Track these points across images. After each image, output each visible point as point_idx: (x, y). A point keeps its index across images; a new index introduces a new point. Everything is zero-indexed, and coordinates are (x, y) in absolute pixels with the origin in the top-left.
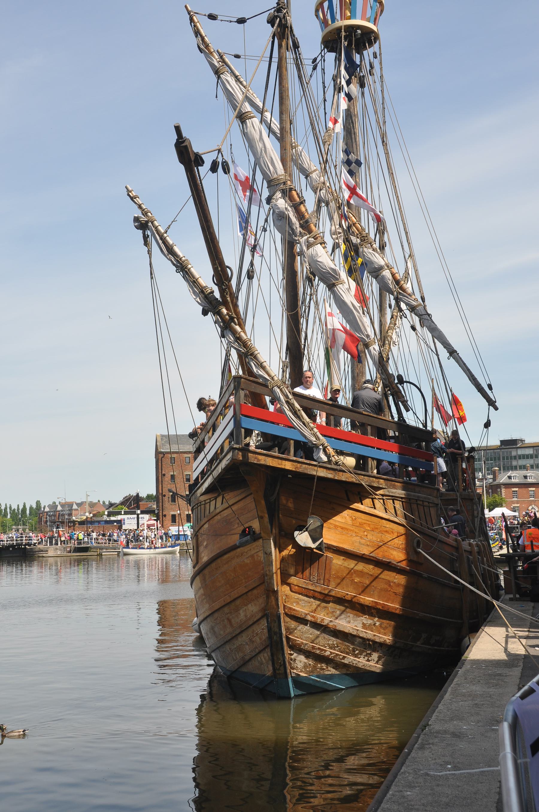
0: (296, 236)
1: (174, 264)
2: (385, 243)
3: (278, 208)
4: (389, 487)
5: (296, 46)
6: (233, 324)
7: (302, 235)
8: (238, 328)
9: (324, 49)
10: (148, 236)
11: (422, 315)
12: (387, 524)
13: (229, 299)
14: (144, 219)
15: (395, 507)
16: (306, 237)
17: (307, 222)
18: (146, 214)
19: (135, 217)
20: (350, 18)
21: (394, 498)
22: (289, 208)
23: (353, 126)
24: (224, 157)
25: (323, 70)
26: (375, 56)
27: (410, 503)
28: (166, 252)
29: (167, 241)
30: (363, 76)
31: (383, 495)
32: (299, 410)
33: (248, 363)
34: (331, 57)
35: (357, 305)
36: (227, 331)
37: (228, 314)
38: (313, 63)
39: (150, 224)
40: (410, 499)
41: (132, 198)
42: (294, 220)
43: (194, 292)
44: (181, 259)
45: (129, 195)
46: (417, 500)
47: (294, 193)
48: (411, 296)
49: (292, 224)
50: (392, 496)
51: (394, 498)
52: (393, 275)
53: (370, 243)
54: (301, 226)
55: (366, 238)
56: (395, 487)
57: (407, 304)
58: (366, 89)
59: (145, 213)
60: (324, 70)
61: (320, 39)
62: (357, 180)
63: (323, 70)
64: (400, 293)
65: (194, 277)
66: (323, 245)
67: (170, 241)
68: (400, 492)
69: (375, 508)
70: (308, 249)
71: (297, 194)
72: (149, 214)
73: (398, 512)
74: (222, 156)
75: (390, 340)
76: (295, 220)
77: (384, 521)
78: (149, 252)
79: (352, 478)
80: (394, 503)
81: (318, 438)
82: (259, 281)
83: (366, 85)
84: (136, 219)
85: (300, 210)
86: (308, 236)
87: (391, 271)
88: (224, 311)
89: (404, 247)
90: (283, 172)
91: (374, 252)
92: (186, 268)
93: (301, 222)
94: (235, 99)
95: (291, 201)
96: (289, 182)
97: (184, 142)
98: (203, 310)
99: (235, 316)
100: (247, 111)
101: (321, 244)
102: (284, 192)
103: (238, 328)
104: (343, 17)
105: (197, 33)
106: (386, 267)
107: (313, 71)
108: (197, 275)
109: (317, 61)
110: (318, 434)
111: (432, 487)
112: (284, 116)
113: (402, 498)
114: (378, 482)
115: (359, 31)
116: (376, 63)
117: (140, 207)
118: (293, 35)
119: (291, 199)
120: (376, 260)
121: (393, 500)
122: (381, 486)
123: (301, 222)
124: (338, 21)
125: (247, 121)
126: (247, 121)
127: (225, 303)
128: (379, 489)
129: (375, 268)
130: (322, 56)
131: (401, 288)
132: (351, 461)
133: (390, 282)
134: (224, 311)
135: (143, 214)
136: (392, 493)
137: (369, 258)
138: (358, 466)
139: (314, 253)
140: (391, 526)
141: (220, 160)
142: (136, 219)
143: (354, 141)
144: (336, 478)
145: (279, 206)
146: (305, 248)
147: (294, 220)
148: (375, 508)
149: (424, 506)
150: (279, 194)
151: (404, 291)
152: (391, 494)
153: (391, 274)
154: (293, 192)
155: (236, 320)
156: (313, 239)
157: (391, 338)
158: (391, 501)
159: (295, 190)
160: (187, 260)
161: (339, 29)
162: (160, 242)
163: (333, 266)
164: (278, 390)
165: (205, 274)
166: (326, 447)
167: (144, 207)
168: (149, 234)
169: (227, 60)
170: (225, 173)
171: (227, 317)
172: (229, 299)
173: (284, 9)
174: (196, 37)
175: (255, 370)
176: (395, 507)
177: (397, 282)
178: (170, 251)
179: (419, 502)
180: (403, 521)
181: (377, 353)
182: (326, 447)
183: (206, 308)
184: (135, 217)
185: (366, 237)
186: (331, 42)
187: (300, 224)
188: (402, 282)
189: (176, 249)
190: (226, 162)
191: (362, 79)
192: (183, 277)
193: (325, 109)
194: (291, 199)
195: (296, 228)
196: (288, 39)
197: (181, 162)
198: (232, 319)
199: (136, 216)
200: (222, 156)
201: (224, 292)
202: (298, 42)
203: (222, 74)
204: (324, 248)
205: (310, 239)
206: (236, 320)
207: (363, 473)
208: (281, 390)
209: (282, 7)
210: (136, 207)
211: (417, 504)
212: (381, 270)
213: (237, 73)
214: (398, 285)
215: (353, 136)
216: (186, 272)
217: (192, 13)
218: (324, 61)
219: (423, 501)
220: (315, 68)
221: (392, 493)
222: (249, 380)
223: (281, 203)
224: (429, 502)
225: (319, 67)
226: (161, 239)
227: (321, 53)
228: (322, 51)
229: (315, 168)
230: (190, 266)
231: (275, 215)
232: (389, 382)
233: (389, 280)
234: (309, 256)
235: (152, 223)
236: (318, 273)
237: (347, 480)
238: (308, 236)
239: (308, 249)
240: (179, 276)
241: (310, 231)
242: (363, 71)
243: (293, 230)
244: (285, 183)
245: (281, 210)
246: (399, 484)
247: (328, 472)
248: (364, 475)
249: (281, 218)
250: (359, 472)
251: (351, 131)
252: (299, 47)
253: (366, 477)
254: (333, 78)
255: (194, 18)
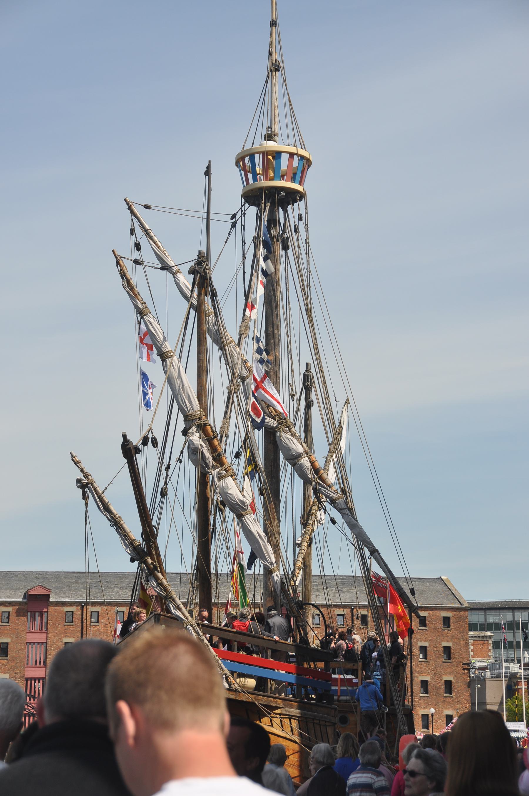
0: (209, 469)
1: (109, 519)
2: (313, 401)
3: (194, 444)
4: (286, 707)
5: (214, 295)
6: (156, 572)
7: (214, 468)
8: (160, 575)
9: (244, 204)
10: (87, 492)
11: (342, 509)
12: (283, 742)
13: (154, 552)
14: (85, 481)
15: (291, 727)
16: (218, 470)
17: (219, 455)
18: (87, 477)
19: (77, 479)
20: (272, 179)
21: (291, 717)
22: (203, 444)
23: (274, 294)
24: (154, 434)
25: (243, 226)
26: (300, 218)
27: (307, 722)
28: (102, 508)
29: (104, 500)
30: (287, 238)
31: (280, 714)
32: (207, 645)
33: (168, 604)
34: (252, 211)
35: (263, 534)
36: (151, 577)
37: (152, 563)
38: (232, 218)
39: (90, 485)
40: (306, 718)
41: (76, 463)
42: (207, 454)
43: (125, 544)
44: (115, 516)
45: (73, 460)
46: (313, 719)
47: (208, 427)
48: (330, 487)
49: (206, 458)
50: (289, 715)
51: (291, 717)
52: (312, 463)
53: (288, 427)
54: (214, 459)
55: (284, 421)
56: (291, 707)
57: (327, 497)
58: (290, 252)
59: (86, 476)
60: (244, 226)
61: (240, 193)
62: (277, 354)
63: (243, 226)
64: (319, 483)
65: (125, 532)
66: (234, 477)
67: (106, 500)
68: (296, 712)
69: (272, 726)
70: (219, 480)
71: (211, 428)
72: (90, 477)
73: (295, 731)
74: (152, 433)
75: (313, 519)
76: (209, 454)
77: (280, 739)
78: (86, 504)
79: (250, 698)
80: (291, 723)
81: (222, 668)
82: (172, 513)
83: (290, 247)
84: (79, 481)
85: (214, 444)
86: (220, 469)
87: (309, 459)
88: (150, 561)
89: (245, 672)
90: (199, 407)
91: (292, 438)
92: (119, 523)
93: (214, 455)
94: (156, 339)
95: (206, 436)
96: (204, 417)
97: (128, 445)
98: (131, 558)
99: (158, 566)
100: (167, 350)
101: (231, 476)
102: (198, 426)
103: (160, 575)
104: (267, 177)
105: (123, 275)
106: (305, 455)
107: (231, 229)
108: (128, 531)
109: (237, 217)
110: (222, 665)
111: (329, 706)
112: (201, 356)
113: (298, 717)
114: (276, 702)
115: (283, 193)
116: (301, 226)
117: (82, 470)
118: (211, 285)
119: (205, 433)
120: (294, 447)
121: (290, 719)
122: (279, 706)
123: (214, 455)
124: (260, 180)
125: (167, 360)
126: (167, 360)
127: (150, 554)
128: (277, 708)
129: (293, 455)
130: (242, 211)
131: (321, 478)
132: (251, 683)
133: (308, 472)
134: (150, 561)
135: (84, 476)
136: (289, 712)
137: (286, 444)
138: (257, 688)
139: (225, 485)
140: (287, 744)
141: (150, 436)
142: (79, 481)
143: (274, 310)
144: (237, 699)
145: (195, 442)
146: (216, 480)
147: (207, 454)
148: (272, 726)
149: (320, 725)
150: (194, 429)
151: (323, 481)
152: (288, 713)
153: (310, 461)
154: (208, 426)
155: (159, 569)
156: (224, 472)
157: (316, 516)
158: (288, 720)
159: (210, 425)
160: (120, 517)
161: (261, 189)
162: (98, 501)
163: (242, 498)
164: (191, 628)
165: (136, 531)
166: (228, 676)
167: (85, 470)
168: (88, 491)
169: (136, 211)
170: (154, 446)
171: (152, 566)
172: (154, 552)
173: (204, 262)
174: (123, 279)
175: (173, 610)
176: (291, 727)
177: (316, 471)
178: (106, 508)
179: (315, 721)
180: (296, 738)
181: (279, 580)
182: (228, 676)
183: (135, 558)
184: (77, 479)
185: (285, 419)
186: (252, 197)
187: (213, 456)
188: (322, 471)
189: (112, 507)
190: (155, 438)
191: (285, 240)
192: (116, 531)
193: (244, 269)
194: (205, 433)
195: (209, 462)
196: (207, 287)
197: (125, 456)
198: (155, 568)
199: (79, 478)
200: (152, 433)
201: (150, 547)
202: (216, 292)
203: (145, 315)
204: (234, 480)
205: (222, 472)
206: (159, 569)
207: (262, 693)
208: (193, 628)
209: (202, 261)
210: (79, 470)
211: (314, 723)
212: (298, 458)
213: (148, 227)
214: (317, 474)
215: (274, 305)
216: (119, 526)
217: (119, 258)
218: (244, 216)
219: (319, 720)
220: (234, 225)
221: (289, 712)
222: (167, 617)
223: (196, 437)
224: (326, 722)
225: (239, 225)
226: (99, 498)
227: (241, 208)
228: (242, 206)
229: (231, 339)
230: (122, 522)
231: (190, 449)
232: (290, 607)
233: (308, 469)
234: (220, 488)
235: (92, 484)
236: (227, 502)
237: (247, 700)
238: (220, 469)
239: (219, 480)
240: (113, 530)
241: (222, 464)
242: (287, 232)
243: (206, 464)
244: (200, 419)
245: (196, 446)
246: (296, 704)
247: (231, 693)
248: (263, 696)
249: (195, 453)
250: (259, 693)
251: (271, 299)
252: (217, 296)
253: (264, 698)
254: (253, 240)
255: (121, 262)
